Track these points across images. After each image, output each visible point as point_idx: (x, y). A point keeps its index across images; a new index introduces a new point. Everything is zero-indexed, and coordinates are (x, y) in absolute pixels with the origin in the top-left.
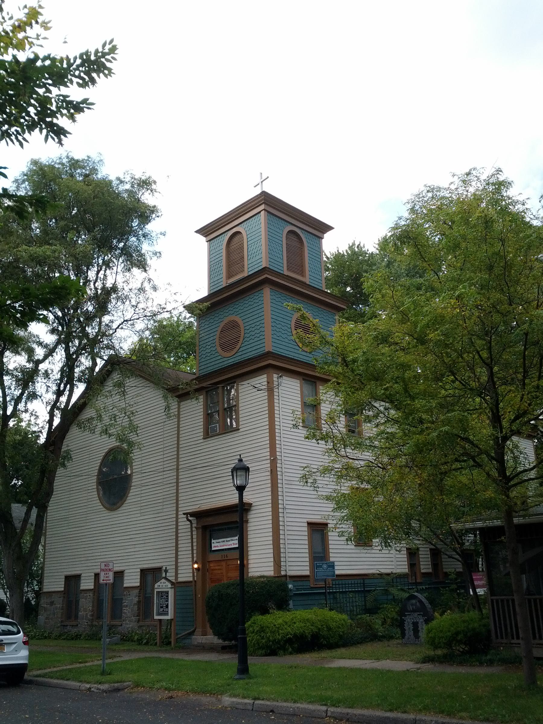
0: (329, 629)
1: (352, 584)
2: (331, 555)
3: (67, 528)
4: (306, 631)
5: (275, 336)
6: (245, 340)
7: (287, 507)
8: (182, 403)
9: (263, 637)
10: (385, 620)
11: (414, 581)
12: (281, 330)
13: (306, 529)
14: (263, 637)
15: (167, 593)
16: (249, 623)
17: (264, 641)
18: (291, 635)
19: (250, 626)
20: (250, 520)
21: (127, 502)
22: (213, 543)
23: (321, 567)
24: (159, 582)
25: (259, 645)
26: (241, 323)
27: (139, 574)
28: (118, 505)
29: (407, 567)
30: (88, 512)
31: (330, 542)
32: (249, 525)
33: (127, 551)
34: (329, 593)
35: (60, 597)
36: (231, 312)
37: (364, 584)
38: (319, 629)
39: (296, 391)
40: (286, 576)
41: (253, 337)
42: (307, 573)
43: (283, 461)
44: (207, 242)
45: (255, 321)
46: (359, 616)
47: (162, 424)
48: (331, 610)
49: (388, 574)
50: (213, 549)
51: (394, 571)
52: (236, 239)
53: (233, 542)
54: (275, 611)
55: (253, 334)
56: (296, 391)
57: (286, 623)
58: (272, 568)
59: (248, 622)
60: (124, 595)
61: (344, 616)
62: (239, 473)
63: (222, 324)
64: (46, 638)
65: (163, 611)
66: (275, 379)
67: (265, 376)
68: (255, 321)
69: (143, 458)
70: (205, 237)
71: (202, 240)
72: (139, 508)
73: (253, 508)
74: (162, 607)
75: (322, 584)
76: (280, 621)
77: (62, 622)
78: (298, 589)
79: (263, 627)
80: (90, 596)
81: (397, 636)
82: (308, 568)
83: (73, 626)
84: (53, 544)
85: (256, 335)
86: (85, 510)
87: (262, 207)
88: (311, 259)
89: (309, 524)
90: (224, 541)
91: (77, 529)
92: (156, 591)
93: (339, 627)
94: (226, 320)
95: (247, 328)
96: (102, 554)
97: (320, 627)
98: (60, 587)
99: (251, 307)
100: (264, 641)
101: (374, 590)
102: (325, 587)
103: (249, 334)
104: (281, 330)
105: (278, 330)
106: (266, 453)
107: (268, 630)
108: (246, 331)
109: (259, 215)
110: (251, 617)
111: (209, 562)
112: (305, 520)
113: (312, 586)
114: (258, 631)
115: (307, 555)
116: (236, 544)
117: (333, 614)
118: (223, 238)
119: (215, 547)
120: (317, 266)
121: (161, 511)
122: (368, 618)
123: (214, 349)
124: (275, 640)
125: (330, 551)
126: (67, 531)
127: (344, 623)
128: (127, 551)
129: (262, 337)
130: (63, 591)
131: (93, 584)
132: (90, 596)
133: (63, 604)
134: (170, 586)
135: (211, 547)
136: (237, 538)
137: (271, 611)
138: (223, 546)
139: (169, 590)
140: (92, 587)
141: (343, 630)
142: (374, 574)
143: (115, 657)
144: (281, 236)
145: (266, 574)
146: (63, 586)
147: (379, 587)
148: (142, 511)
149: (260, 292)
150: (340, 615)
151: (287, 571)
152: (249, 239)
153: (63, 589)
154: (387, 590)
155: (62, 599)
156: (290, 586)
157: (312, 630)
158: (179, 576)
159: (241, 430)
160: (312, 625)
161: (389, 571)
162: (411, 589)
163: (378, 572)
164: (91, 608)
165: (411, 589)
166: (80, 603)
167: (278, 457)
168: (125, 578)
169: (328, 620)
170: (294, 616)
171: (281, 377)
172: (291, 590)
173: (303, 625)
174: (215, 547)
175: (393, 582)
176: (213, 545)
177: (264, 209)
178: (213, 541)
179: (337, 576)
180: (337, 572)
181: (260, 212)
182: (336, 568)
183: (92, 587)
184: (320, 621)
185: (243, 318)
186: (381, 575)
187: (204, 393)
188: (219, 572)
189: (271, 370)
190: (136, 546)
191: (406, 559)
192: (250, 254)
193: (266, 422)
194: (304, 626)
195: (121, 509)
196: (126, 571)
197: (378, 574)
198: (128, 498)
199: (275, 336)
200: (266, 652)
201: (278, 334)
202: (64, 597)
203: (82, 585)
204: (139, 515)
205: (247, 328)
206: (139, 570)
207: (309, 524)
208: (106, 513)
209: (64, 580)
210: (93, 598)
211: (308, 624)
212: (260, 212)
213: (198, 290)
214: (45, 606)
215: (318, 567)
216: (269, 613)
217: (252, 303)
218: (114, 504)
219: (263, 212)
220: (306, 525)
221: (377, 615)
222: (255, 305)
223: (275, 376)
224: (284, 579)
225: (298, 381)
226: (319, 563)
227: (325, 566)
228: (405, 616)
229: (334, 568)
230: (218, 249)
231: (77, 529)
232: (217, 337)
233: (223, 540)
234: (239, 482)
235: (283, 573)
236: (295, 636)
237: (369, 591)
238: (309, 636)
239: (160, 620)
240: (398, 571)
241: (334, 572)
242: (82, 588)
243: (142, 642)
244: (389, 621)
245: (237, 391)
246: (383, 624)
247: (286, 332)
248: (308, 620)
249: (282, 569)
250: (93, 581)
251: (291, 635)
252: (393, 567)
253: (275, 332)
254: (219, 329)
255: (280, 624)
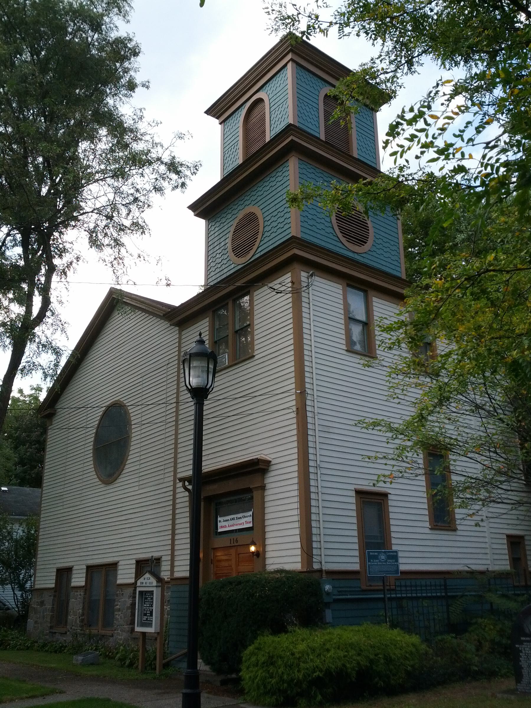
0: (388, 660)
1: (426, 586)
2: (394, 541)
3: (61, 508)
4: (348, 665)
5: (305, 225)
6: (264, 236)
7: (323, 465)
8: (183, 333)
9: (272, 673)
10: (480, 643)
11: (523, 583)
12: (315, 217)
13: (353, 500)
14: (272, 673)
15: (152, 593)
16: (251, 648)
17: (274, 681)
18: (321, 671)
19: (252, 654)
20: (268, 486)
21: (124, 472)
22: (220, 521)
23: (376, 557)
24: (142, 578)
25: (265, 687)
26: (259, 214)
27: (134, 566)
28: (115, 475)
29: (508, 563)
30: (83, 487)
31: (392, 522)
32: (267, 493)
33: (123, 536)
34: (390, 599)
35: (50, 596)
36: (247, 203)
37: (445, 585)
38: (371, 661)
39: (337, 300)
40: (320, 571)
41: (275, 230)
42: (356, 567)
43: (315, 397)
44: (220, 124)
45: (277, 206)
46: (439, 638)
47: (165, 367)
48: (393, 626)
49: (482, 573)
50: (220, 530)
51: (491, 569)
52: (256, 111)
53: (246, 519)
54: (297, 629)
55: (275, 224)
56: (337, 300)
57: (313, 650)
58: (299, 559)
59: (250, 645)
60: (117, 595)
61: (415, 639)
62: (194, 364)
63: (237, 221)
64: (28, 648)
65: (147, 619)
66: (303, 279)
67: (289, 275)
68: (277, 206)
69: (143, 414)
70: (217, 118)
71: (214, 123)
72: (137, 479)
73: (273, 468)
74: (145, 615)
75: (379, 585)
76: (302, 647)
77: (51, 627)
78: (340, 593)
79: (272, 657)
80: (80, 595)
81: (503, 671)
82: (357, 560)
83: (61, 633)
84: (47, 529)
85: (279, 225)
86: (81, 485)
87: (289, 57)
88: (360, 134)
89: (358, 492)
90: (233, 519)
91: (71, 509)
92: (138, 589)
93: (406, 658)
94: (240, 215)
95: (267, 219)
96: (96, 540)
97: (372, 657)
98: (50, 583)
99: (274, 188)
100: (274, 681)
101: (462, 596)
102: (383, 590)
103: (270, 227)
104: (315, 217)
105: (310, 217)
106: (291, 385)
107: (280, 662)
108: (266, 223)
109: (286, 68)
110: (256, 638)
111: (214, 549)
112: (353, 487)
113: (364, 587)
114: (264, 663)
115: (356, 540)
116: (250, 523)
117: (396, 634)
118: (240, 113)
119: (222, 527)
120: (370, 144)
121: (162, 481)
122: (455, 641)
123: (226, 256)
124: (292, 680)
125: (393, 535)
126: (62, 511)
127: (414, 650)
128: (123, 536)
129: (287, 226)
130: (53, 588)
131: (84, 579)
132: (80, 595)
133: (53, 605)
134: (155, 583)
135: (217, 528)
136: (251, 513)
137: (290, 628)
138: (232, 526)
139: (154, 589)
140: (83, 584)
141: (412, 663)
142: (459, 572)
143: (53, 692)
144: (317, 97)
145: (287, 567)
146: (54, 581)
147: (469, 591)
148: (141, 483)
149: (283, 166)
150: (407, 637)
151: (323, 563)
152: (272, 105)
153: (53, 586)
154: (481, 596)
155: (52, 598)
156: (327, 587)
157: (358, 663)
158: (176, 569)
159: (256, 357)
160: (359, 655)
161: (482, 568)
162: (518, 595)
163: (466, 569)
164: (80, 611)
165: (518, 595)
166: (70, 604)
167: (308, 391)
168: (119, 572)
169: (386, 646)
170: (327, 637)
171: (312, 275)
172: (328, 594)
173: (341, 654)
174: (222, 527)
175: (489, 584)
176: (219, 525)
177: (292, 60)
178: (219, 519)
179: (403, 573)
180: (402, 568)
181: (286, 65)
182: (401, 560)
183: (83, 584)
184: (372, 647)
185: (262, 207)
186: (472, 573)
187: (210, 314)
188: (226, 564)
189: (296, 266)
190: (133, 529)
191: (506, 552)
192: (273, 122)
193: (290, 341)
194: (345, 656)
195: (118, 481)
196: (120, 563)
197: (467, 572)
198: (127, 467)
199: (305, 225)
200: (277, 699)
201: (311, 222)
202: (55, 596)
203: (73, 580)
204: (137, 488)
205: (267, 219)
206: (134, 562)
207: (358, 492)
208: (103, 488)
209: (55, 574)
210: (84, 598)
211: (352, 652)
212: (286, 65)
213: (181, 137)
214: (36, 606)
215: (371, 557)
216: (286, 632)
217: (275, 183)
218: (110, 476)
219: (290, 65)
220: (353, 494)
221: (467, 634)
222: (279, 184)
223: (303, 274)
224: (316, 576)
225: (340, 287)
226: (373, 552)
227: (383, 557)
228: (521, 643)
229: (397, 561)
230: (234, 128)
231: (71, 509)
232: (229, 241)
233: (232, 516)
234: (194, 381)
235: (316, 566)
236: (328, 673)
237: (454, 597)
238: (354, 674)
239: (144, 634)
240: (497, 568)
241: (398, 565)
242: (73, 584)
243: (125, 663)
244: (487, 646)
245: (251, 301)
246: (477, 650)
247: (323, 221)
248: (351, 645)
249: (314, 560)
250: (84, 575)
251: (321, 671)
252: (488, 562)
253: (306, 219)
254: (232, 229)
255: (302, 653)
